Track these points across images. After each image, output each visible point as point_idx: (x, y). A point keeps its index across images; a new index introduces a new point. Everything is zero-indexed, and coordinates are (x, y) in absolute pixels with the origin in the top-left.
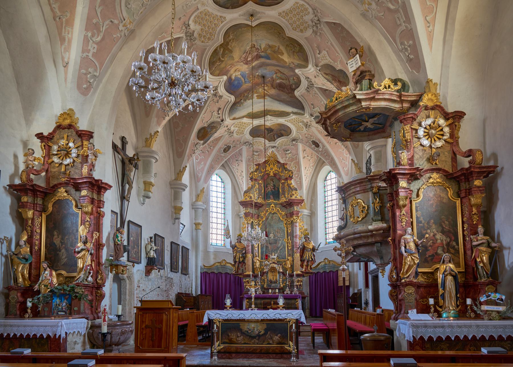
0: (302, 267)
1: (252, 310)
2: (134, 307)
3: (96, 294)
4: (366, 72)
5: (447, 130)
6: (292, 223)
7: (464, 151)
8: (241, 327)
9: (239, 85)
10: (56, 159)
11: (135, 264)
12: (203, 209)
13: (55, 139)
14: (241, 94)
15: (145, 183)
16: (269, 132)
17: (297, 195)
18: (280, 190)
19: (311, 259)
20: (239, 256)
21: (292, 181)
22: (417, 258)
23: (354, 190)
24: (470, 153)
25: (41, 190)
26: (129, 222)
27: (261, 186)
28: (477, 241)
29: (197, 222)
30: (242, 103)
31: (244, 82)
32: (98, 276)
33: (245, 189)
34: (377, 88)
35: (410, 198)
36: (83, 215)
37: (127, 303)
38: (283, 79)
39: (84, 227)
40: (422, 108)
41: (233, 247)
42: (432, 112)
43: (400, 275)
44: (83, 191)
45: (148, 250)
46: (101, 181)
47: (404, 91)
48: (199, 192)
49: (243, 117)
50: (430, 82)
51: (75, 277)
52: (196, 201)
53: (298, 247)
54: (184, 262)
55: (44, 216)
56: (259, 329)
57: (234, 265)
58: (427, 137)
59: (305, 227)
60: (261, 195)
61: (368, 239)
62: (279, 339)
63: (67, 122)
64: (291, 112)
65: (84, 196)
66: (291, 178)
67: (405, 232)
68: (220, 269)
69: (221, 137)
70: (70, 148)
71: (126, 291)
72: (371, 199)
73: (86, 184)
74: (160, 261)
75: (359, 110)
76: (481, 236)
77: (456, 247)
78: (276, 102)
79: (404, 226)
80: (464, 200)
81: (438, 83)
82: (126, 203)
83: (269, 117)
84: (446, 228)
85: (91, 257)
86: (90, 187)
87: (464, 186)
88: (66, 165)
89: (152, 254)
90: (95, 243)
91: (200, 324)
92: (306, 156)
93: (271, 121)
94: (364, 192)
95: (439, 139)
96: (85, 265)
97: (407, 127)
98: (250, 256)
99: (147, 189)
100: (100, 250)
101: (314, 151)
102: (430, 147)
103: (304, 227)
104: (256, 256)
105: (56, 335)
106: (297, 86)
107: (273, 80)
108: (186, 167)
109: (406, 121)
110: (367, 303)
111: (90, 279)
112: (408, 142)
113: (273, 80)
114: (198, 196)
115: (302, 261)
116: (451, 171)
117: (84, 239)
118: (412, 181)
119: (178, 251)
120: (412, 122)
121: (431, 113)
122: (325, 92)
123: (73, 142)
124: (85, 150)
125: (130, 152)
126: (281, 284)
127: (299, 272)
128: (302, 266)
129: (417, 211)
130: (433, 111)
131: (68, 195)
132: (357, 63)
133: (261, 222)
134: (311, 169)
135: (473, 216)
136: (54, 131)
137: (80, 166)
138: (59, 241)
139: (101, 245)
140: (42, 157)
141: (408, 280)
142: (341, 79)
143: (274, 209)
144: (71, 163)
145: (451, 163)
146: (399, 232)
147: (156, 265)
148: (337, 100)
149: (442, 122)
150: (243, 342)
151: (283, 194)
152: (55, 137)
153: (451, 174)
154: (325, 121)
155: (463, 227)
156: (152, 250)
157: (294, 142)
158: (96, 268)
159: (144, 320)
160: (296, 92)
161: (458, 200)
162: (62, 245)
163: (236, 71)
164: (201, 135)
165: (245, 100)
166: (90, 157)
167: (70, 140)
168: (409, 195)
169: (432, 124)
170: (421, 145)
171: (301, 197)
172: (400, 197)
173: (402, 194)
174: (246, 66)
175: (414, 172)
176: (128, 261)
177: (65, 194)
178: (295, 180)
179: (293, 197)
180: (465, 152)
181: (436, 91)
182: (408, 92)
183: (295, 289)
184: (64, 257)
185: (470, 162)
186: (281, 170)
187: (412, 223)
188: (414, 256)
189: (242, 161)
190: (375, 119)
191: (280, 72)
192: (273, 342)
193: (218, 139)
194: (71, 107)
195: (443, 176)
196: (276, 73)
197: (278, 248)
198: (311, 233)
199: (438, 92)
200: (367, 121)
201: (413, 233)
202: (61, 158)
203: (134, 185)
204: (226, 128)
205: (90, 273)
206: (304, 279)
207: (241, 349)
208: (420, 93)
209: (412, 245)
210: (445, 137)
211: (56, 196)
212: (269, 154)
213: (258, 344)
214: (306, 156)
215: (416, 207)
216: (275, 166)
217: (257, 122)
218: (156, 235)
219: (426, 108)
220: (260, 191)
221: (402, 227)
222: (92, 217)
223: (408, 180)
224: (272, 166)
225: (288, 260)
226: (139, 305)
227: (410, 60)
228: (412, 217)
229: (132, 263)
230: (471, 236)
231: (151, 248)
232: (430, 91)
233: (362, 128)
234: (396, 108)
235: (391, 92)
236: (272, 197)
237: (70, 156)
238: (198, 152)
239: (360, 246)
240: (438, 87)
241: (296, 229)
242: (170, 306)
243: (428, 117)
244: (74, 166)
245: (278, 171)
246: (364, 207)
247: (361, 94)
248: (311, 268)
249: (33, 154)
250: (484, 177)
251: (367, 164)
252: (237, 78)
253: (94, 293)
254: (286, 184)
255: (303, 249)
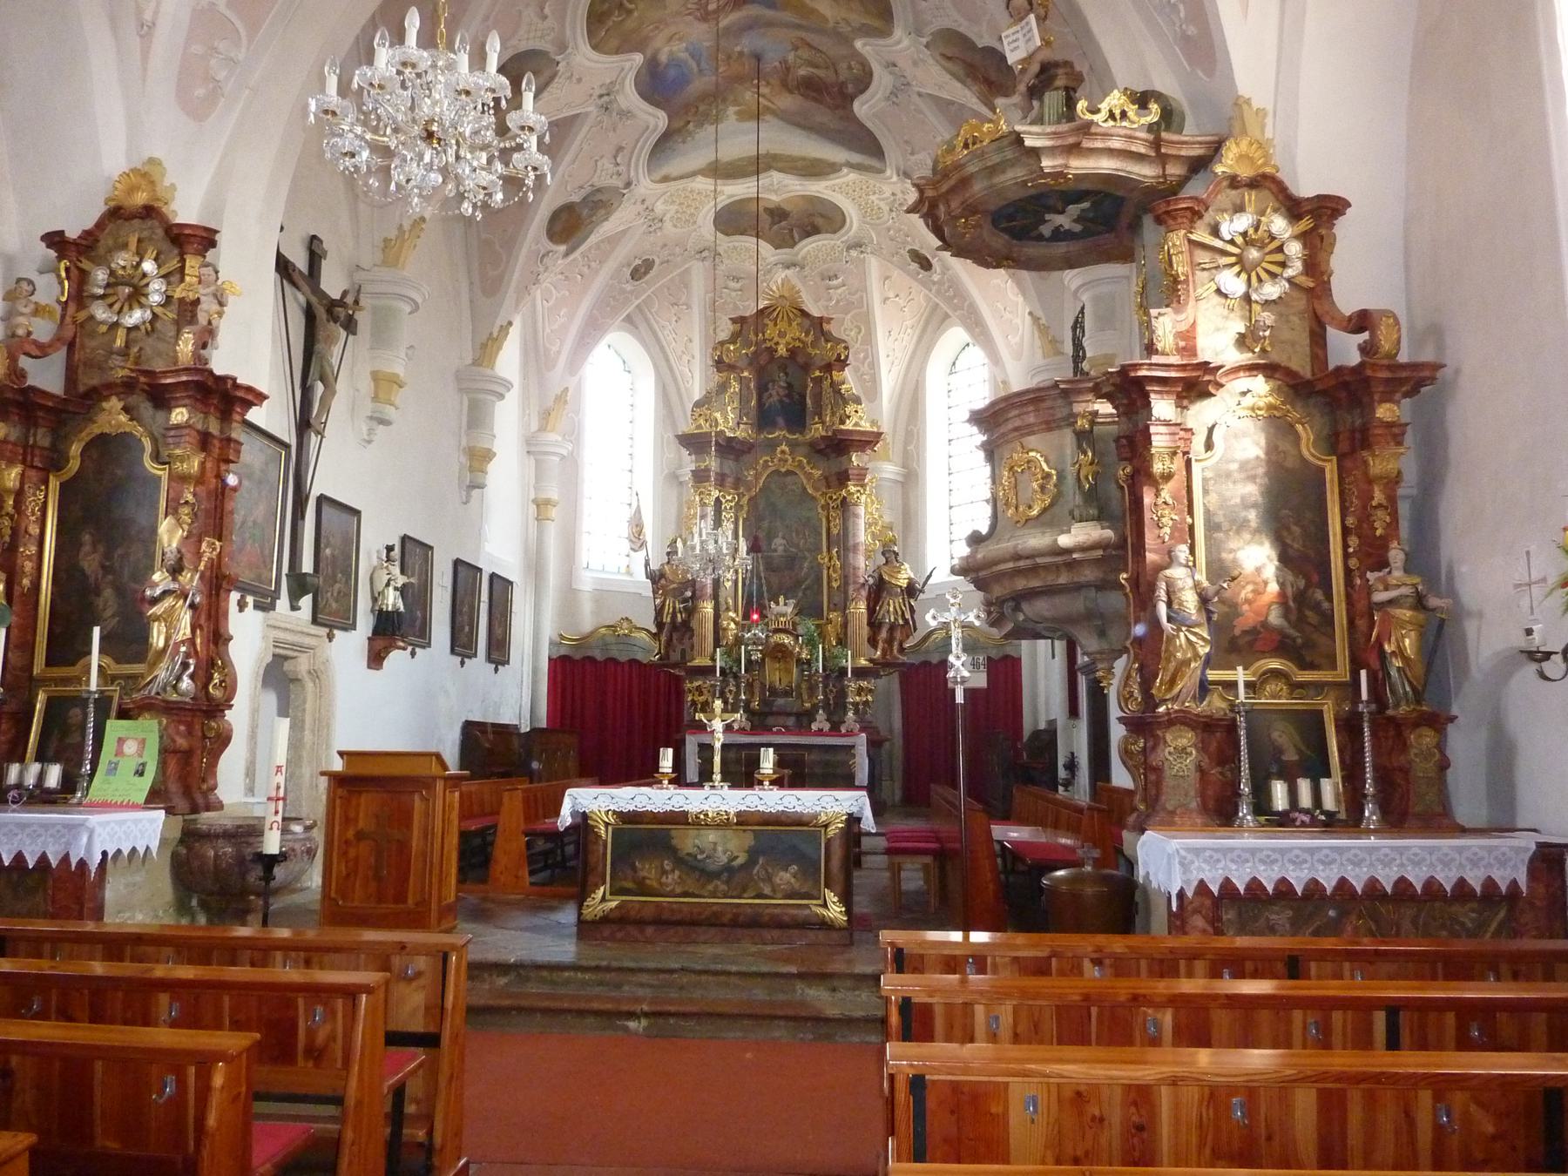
0: (875, 646)
1: (713, 787)
2: (323, 774)
3: (203, 731)
4: (1056, 65)
5: (1294, 249)
6: (845, 505)
7: (1348, 314)
8: (674, 842)
9: (683, 81)
10: (101, 313)
11: (335, 632)
12: (563, 457)
13: (101, 250)
14: (687, 107)
15: (376, 377)
16: (777, 219)
17: (861, 418)
18: (809, 401)
19: (901, 622)
20: (674, 608)
21: (847, 372)
22: (1203, 639)
23: (1018, 423)
24: (1362, 321)
25: (50, 404)
26: (322, 499)
27: (749, 388)
28: (1386, 589)
29: (544, 496)
30: (690, 133)
31: (696, 70)
32: (212, 675)
33: (697, 397)
34: (1089, 117)
35: (1185, 453)
36: (174, 484)
37: (305, 754)
38: (817, 67)
39: (173, 521)
40: (1220, 183)
41: (656, 578)
42: (1250, 195)
43: (1154, 691)
44: (178, 410)
45: (380, 586)
46: (234, 380)
47: (1168, 129)
48: (550, 403)
49: (693, 174)
50: (1245, 107)
51: (142, 676)
52: (542, 429)
53: (862, 580)
54: (496, 623)
55: (54, 484)
56: (728, 848)
57: (655, 636)
58: (1237, 269)
59: (887, 519)
60: (747, 415)
61: (1058, 577)
62: (793, 880)
63: (140, 198)
64: (843, 161)
65: (178, 427)
66: (842, 363)
67: (1171, 560)
68: (614, 647)
69: (624, 232)
70: (144, 275)
71: (303, 716)
72: (1069, 452)
73: (186, 390)
74: (418, 623)
75: (1032, 181)
76: (1398, 574)
77: (1326, 605)
78: (799, 131)
79: (1167, 538)
80: (1348, 464)
81: (1270, 108)
82: (314, 440)
83: (776, 177)
84: (1296, 546)
85: (192, 618)
86: (197, 400)
87: (1351, 419)
88: (129, 330)
89: (392, 600)
90: (208, 574)
91: (545, 824)
92: (891, 295)
93: (781, 188)
94: (1050, 429)
95: (1273, 275)
96: (172, 643)
97: (1177, 239)
98: (708, 608)
99: (381, 395)
100: (223, 594)
101: (917, 280)
102: (1247, 298)
103: (881, 517)
104: (728, 609)
105: (67, 855)
106: (861, 87)
107: (788, 69)
108: (510, 324)
109: (1175, 219)
110: (1072, 766)
111: (186, 683)
112: (1179, 282)
113: (787, 69)
114: (546, 416)
115: (874, 624)
116: (1308, 374)
117: (171, 558)
118: (1192, 402)
119: (474, 591)
120: (1192, 221)
121: (1247, 197)
122: (943, 105)
123: (156, 260)
124: (191, 285)
125: (333, 283)
126: (805, 697)
127: (863, 662)
128: (873, 642)
129: (1206, 492)
130: (1254, 193)
131: (131, 420)
132: (1029, 40)
133: (745, 500)
134: (906, 337)
135: (1372, 512)
136: (100, 225)
137: (173, 333)
138: (96, 563)
139: (225, 577)
140: (59, 302)
141: (1176, 707)
142: (993, 76)
143: (786, 461)
144: (144, 323)
145: (1308, 349)
146: (1151, 557)
147: (402, 636)
148: (966, 146)
149: (1279, 225)
150: (678, 890)
151: (816, 414)
152: (102, 242)
153: (1309, 382)
154: (933, 205)
155: (1345, 546)
156: (391, 589)
157: (854, 253)
158: (208, 650)
159: (352, 815)
160: (856, 105)
161: (1330, 461)
162: (104, 576)
163: (670, 39)
164: (558, 227)
165: (700, 125)
166: (203, 306)
167: (146, 251)
168: (1181, 443)
169: (1251, 231)
170: (1219, 291)
171: (873, 423)
172: (1153, 451)
173: (1160, 440)
174: (704, 26)
175: (1194, 374)
176: (315, 621)
177: (123, 418)
178: (857, 370)
179: (849, 425)
180: (1350, 318)
181: (1263, 132)
182: (1180, 132)
183: (850, 714)
184: (109, 613)
185: (1364, 349)
186: (810, 338)
187: (1192, 528)
188: (1195, 634)
189: (689, 307)
190: (1086, 205)
191: (809, 45)
192: (774, 891)
193: (614, 240)
194: (156, 155)
195: (1286, 389)
196: (796, 48)
197: (798, 583)
198: (905, 538)
199: (1269, 134)
200: (1062, 212)
201: (1194, 562)
202: (117, 307)
203: (341, 386)
204: (640, 208)
205: (185, 666)
206: (881, 682)
207: (672, 911)
208: (1216, 138)
209: (1190, 600)
210: (1289, 272)
211: (95, 422)
212: (774, 288)
213: (725, 897)
214: (891, 295)
215: (1205, 480)
216: (794, 324)
217: (741, 189)
218: (405, 539)
219: (1234, 182)
220: (744, 400)
221: (1160, 541)
222: (200, 489)
223: (1180, 397)
224: (782, 325)
225: (830, 621)
226: (338, 765)
227: (1186, 39)
228: (1191, 512)
229: (327, 630)
230: (1369, 575)
231: (389, 580)
232: (1244, 132)
233: (1046, 230)
234: (1145, 176)
235: (1129, 132)
236: (780, 421)
237: (143, 300)
238: (547, 280)
239: (1031, 594)
240: (1269, 121)
241: (855, 524)
242: (435, 769)
243: (1239, 209)
244: (153, 330)
245: (803, 342)
246: (1047, 476)
247: (1038, 134)
248: (902, 650)
249: (32, 294)
250: (1407, 395)
251: (1074, 328)
252: (675, 62)
253: (197, 727)
254: (826, 384)
255: (879, 590)
